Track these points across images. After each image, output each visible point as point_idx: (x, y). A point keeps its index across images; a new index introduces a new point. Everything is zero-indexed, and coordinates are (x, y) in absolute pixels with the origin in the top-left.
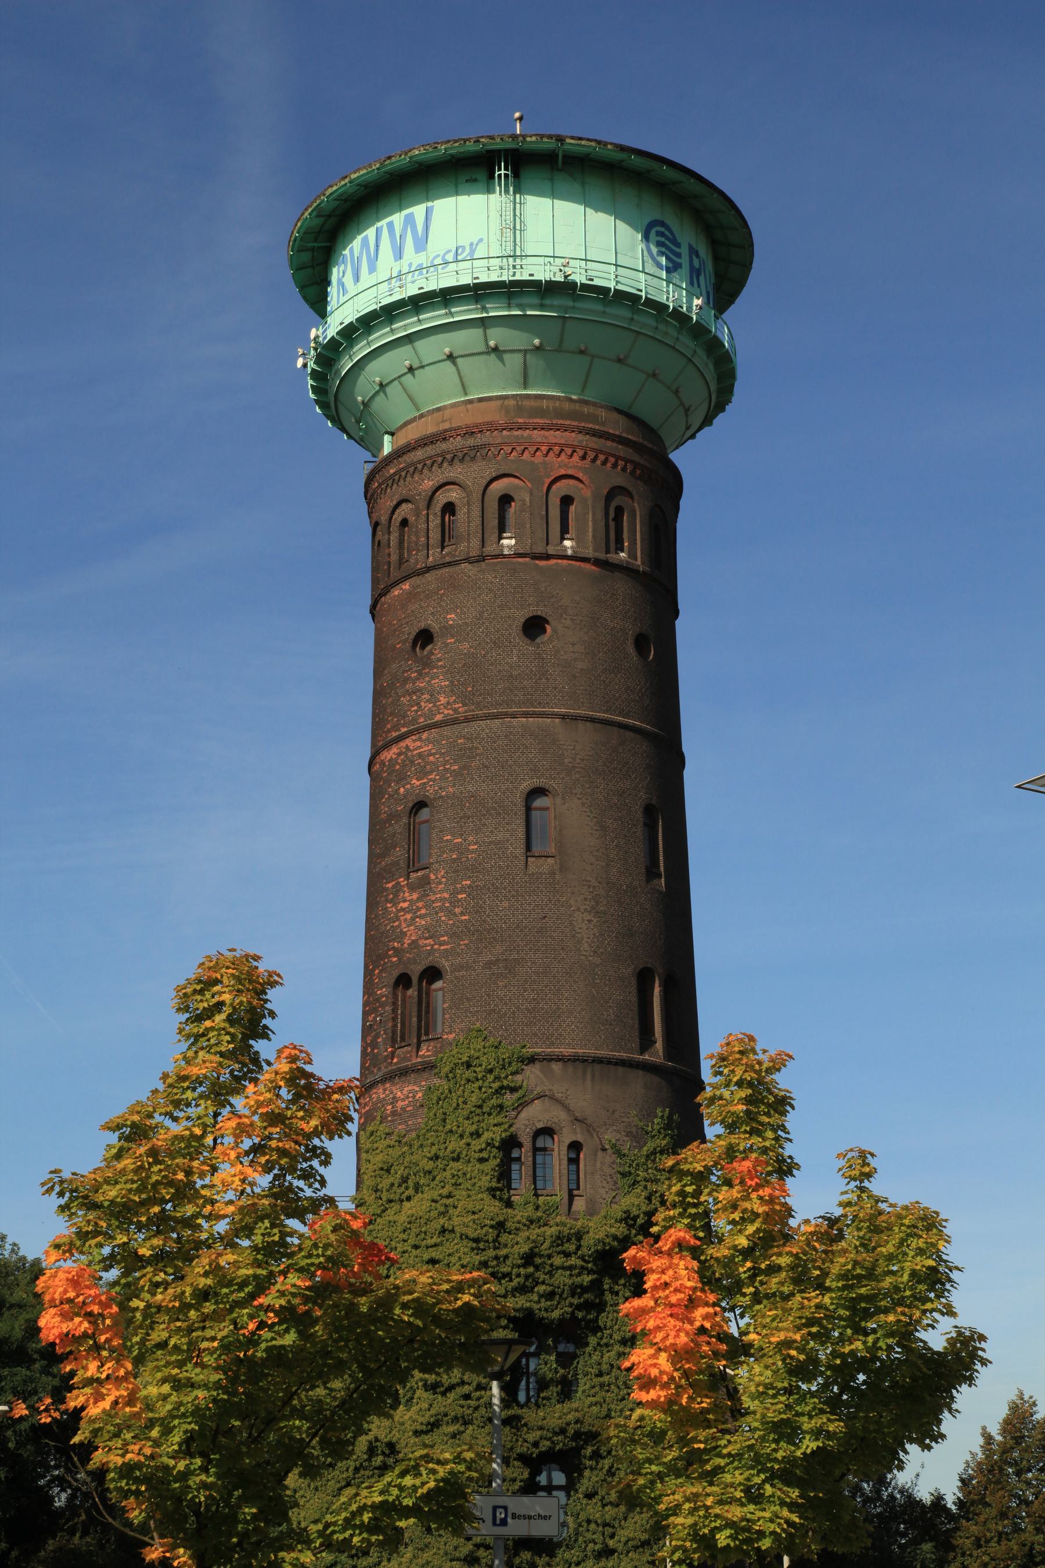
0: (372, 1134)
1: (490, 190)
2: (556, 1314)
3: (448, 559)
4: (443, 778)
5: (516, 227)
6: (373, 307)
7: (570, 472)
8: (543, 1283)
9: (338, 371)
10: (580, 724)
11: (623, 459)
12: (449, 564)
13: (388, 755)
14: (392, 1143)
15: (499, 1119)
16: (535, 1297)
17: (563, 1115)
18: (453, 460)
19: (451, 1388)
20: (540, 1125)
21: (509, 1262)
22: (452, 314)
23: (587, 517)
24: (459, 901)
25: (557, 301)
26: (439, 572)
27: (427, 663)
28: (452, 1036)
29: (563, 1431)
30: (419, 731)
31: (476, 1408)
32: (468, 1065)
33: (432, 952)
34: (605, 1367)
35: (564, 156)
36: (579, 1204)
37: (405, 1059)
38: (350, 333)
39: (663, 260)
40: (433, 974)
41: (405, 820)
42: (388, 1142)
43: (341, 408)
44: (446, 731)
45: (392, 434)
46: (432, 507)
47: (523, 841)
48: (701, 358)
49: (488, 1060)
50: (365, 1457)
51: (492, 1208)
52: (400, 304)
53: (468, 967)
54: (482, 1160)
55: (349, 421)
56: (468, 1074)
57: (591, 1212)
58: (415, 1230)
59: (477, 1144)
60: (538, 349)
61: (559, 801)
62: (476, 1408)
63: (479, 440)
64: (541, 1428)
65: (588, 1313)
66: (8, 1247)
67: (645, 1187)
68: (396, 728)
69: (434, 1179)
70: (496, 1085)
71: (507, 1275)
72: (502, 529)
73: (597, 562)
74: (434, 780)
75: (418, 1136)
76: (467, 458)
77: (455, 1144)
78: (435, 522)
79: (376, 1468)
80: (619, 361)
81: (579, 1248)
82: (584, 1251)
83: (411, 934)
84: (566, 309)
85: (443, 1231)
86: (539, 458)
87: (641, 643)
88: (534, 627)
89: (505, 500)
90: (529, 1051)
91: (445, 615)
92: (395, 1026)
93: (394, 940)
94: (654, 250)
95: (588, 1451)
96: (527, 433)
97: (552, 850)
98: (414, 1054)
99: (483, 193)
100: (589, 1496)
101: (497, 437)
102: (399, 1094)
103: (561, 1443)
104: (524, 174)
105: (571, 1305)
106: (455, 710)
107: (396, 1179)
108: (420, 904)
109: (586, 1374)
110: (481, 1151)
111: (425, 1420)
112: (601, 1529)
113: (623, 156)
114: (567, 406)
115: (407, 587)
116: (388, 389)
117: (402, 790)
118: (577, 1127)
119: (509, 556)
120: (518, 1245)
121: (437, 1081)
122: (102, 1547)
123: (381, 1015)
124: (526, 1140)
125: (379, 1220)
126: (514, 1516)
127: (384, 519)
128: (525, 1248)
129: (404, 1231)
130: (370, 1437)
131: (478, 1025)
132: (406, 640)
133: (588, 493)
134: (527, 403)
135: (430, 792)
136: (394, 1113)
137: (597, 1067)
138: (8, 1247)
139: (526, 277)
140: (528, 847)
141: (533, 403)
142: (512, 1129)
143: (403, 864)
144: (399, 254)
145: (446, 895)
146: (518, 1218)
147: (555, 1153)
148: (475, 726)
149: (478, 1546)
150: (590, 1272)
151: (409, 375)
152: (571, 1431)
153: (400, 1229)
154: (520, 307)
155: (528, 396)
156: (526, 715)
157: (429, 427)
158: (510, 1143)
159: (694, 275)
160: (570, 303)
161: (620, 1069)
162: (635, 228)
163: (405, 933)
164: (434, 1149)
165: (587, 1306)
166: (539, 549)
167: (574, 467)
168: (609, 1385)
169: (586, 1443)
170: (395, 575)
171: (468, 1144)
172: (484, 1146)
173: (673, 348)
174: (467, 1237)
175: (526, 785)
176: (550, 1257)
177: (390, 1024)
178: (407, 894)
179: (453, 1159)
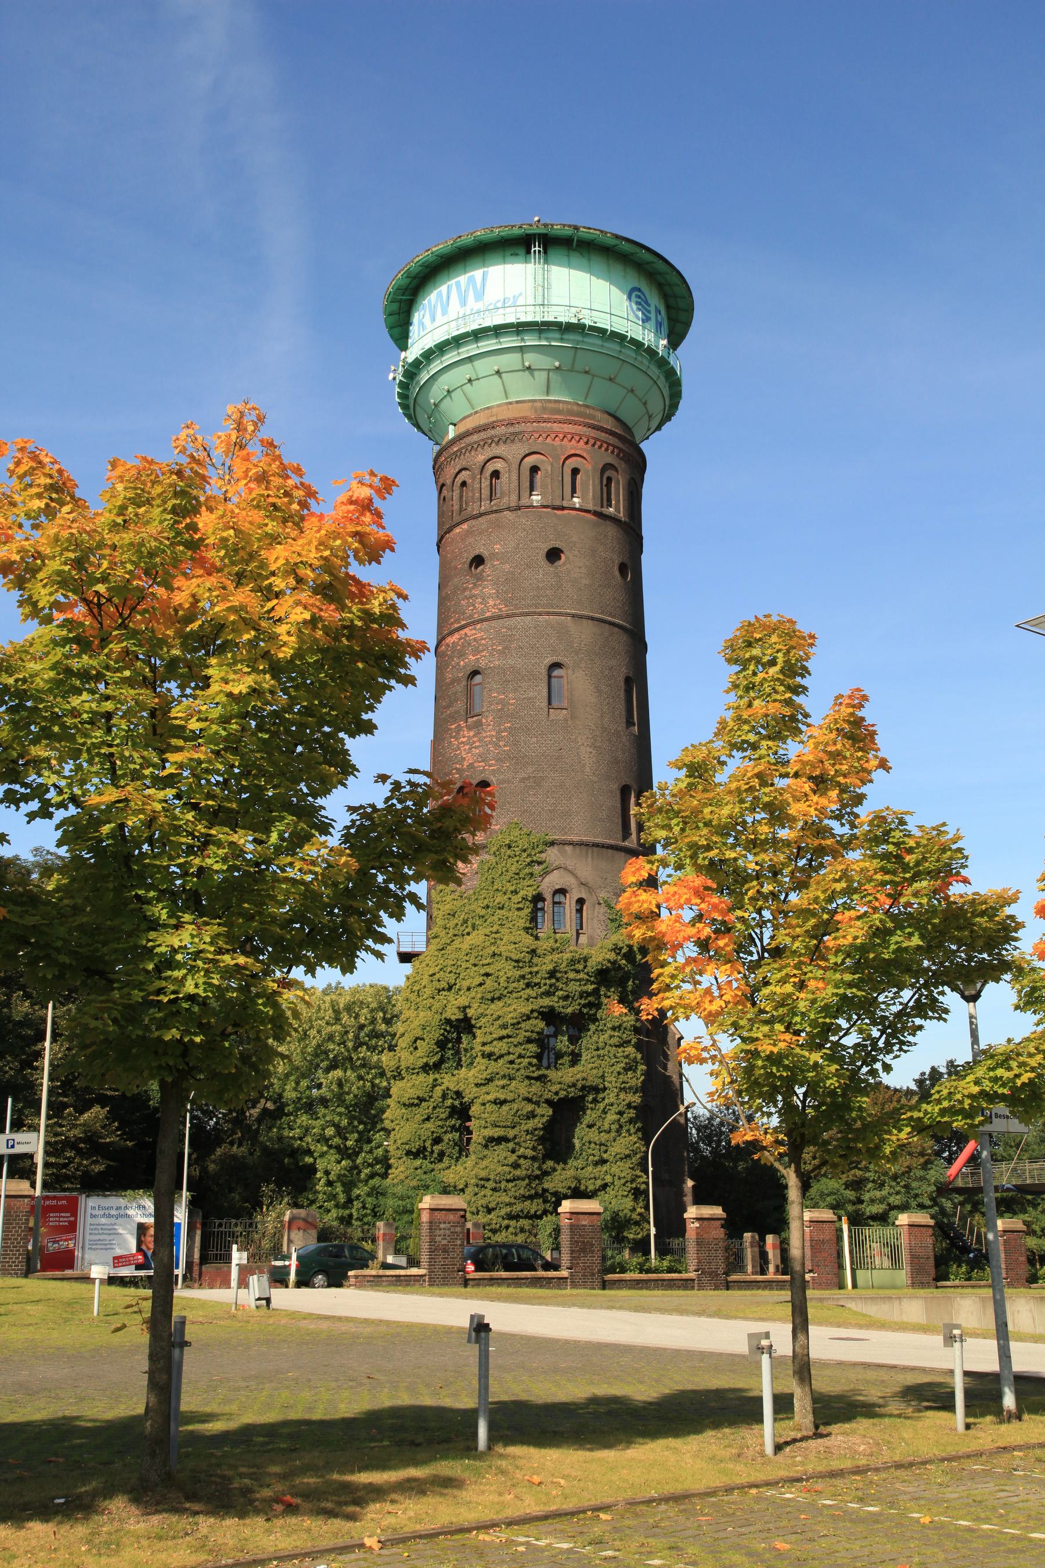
2: (569, 1010)
5: (545, 287)
9: (418, 382)
10: (584, 621)
12: (496, 511)
13: (450, 640)
15: (531, 882)
16: (556, 999)
17: (573, 880)
19: (501, 1056)
27: (480, 578)
29: (574, 1085)
32: (510, 847)
33: (484, 770)
34: (601, 1045)
36: (583, 939)
38: (429, 355)
39: (640, 314)
41: (464, 683)
43: (418, 409)
44: (493, 623)
48: (662, 382)
49: (523, 843)
51: (528, 940)
52: (466, 335)
53: (508, 782)
54: (519, 909)
55: (422, 418)
56: (509, 852)
57: (591, 944)
58: (474, 954)
60: (557, 368)
61: (570, 672)
68: (457, 621)
70: (528, 860)
72: (532, 488)
73: (596, 514)
77: (500, 899)
78: (486, 483)
80: (611, 379)
82: (589, 969)
83: (469, 759)
84: (578, 342)
85: (494, 955)
87: (623, 568)
88: (553, 555)
89: (534, 469)
94: (635, 307)
95: (590, 1098)
97: (565, 705)
100: (590, 1126)
101: (530, 427)
103: (573, 1093)
104: (550, 251)
107: (458, 920)
111: (484, 1076)
114: (575, 408)
120: (545, 965)
121: (487, 857)
122: (251, 1154)
124: (548, 896)
127: (449, 482)
128: (550, 967)
130: (444, 1087)
133: (590, 467)
134: (549, 405)
135: (482, 664)
137: (595, 849)
139: (551, 319)
140: (550, 703)
141: (553, 405)
143: (463, 712)
144: (464, 302)
147: (567, 906)
148: (514, 620)
149: (519, 1157)
150: (592, 983)
152: (579, 1085)
154: (547, 339)
155: (550, 401)
156: (548, 614)
157: (481, 420)
158: (538, 898)
159: (659, 325)
160: (580, 338)
164: (486, 902)
165: (590, 1005)
166: (558, 503)
170: (457, 518)
175: (548, 661)
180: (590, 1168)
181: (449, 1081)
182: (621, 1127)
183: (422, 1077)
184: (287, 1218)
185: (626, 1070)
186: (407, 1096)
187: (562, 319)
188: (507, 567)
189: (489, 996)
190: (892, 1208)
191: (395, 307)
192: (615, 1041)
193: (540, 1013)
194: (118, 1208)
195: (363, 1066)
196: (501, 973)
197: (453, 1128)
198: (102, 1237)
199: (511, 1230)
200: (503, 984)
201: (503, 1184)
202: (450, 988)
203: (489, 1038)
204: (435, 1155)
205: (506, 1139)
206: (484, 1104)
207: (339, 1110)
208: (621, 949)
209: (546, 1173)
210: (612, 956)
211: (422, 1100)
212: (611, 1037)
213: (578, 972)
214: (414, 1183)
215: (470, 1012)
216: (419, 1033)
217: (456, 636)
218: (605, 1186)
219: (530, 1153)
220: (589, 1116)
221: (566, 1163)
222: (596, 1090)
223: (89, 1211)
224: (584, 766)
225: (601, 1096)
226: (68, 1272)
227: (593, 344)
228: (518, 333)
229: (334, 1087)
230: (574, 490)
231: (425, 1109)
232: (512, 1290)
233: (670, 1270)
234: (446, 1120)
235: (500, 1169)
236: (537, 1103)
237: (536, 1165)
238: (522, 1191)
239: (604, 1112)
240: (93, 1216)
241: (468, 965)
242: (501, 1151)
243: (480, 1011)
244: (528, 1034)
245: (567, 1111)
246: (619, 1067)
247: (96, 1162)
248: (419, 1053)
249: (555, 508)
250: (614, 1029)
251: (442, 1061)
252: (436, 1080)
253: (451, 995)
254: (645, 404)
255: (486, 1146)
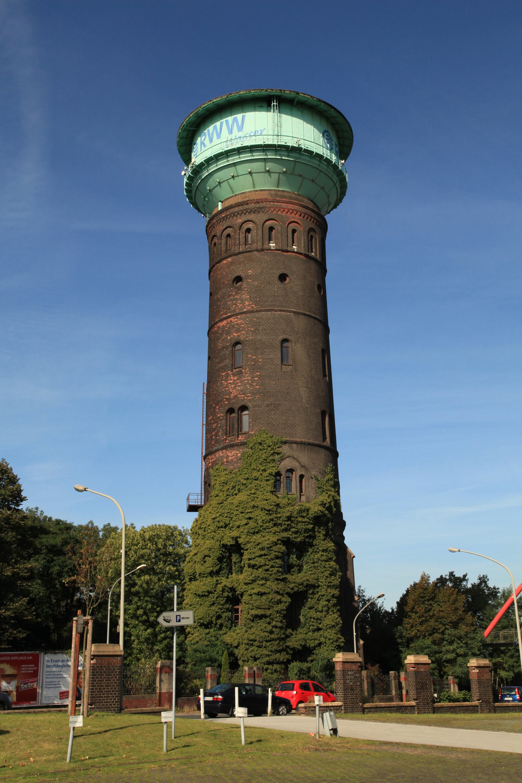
0: (217, 469)
1: (268, 110)
3: (248, 250)
4: (247, 333)
5: (279, 125)
6: (222, 151)
7: (295, 220)
8: (294, 527)
9: (201, 177)
10: (301, 316)
11: (314, 218)
12: (249, 252)
13: (221, 324)
14: (227, 473)
16: (290, 533)
17: (297, 464)
18: (250, 212)
19: (260, 567)
20: (289, 468)
21: (281, 519)
22: (253, 156)
23: (301, 237)
24: (255, 380)
25: (294, 155)
26: (245, 254)
27: (240, 289)
28: (253, 432)
29: (302, 584)
30: (236, 315)
31: (271, 575)
32: (261, 444)
33: (244, 399)
34: (315, 560)
35: (297, 102)
36: (303, 498)
37: (232, 441)
39: (328, 145)
40: (244, 408)
42: (225, 472)
44: (249, 315)
45: (222, 202)
46: (241, 230)
47: (280, 359)
49: (269, 442)
50: (221, 593)
51: (274, 498)
52: (233, 150)
53: (259, 406)
54: (267, 480)
56: (260, 447)
57: (308, 501)
59: (266, 474)
60: (284, 172)
61: (293, 344)
62: (271, 575)
63: (261, 205)
64: (294, 583)
65: (310, 539)
66: (39, 512)
67: (327, 493)
69: (247, 487)
70: (272, 452)
71: (281, 524)
72: (270, 239)
73: (306, 255)
74: (244, 334)
75: (239, 471)
76: (256, 212)
77: (255, 474)
78: (242, 236)
79: (225, 597)
80: (313, 181)
81: (308, 514)
83: (234, 393)
84: (297, 158)
85: (254, 506)
86: (284, 214)
88: (283, 277)
89: (271, 229)
90: (284, 439)
91: (248, 271)
92: (227, 428)
93: (226, 395)
94: (326, 141)
95: (311, 592)
96: (280, 204)
98: (236, 439)
99: (266, 112)
101: (269, 205)
102: (230, 454)
103: (302, 588)
104: (280, 106)
105: (304, 536)
106: (252, 307)
108: (238, 381)
109: (307, 563)
110: (267, 476)
111: (251, 578)
112: (315, 621)
113: (319, 103)
115: (230, 260)
116: (222, 185)
117: (229, 337)
118: (303, 469)
119: (273, 250)
120: (285, 513)
121: (247, 450)
123: (220, 424)
124: (283, 473)
125: (225, 502)
126: (183, 618)
127: (218, 234)
128: (288, 514)
129: (237, 507)
130: (222, 585)
131: (264, 428)
132: (230, 280)
133: (302, 229)
134: (279, 193)
135: (242, 338)
136: (227, 462)
137: (309, 446)
138: (39, 512)
139: (283, 144)
140: (282, 362)
142: (279, 469)
144: (231, 132)
145: (250, 378)
146: (284, 502)
147: (294, 479)
149: (273, 627)
150: (312, 524)
151: (232, 179)
153: (234, 506)
154: (280, 155)
155: (279, 191)
156: (281, 311)
157: (240, 199)
158: (278, 474)
160: (299, 156)
161: (317, 448)
162: (320, 132)
163: (231, 393)
164: (247, 476)
165: (310, 537)
166: (285, 248)
167: (297, 219)
168: (317, 567)
169: (310, 589)
170: (224, 255)
171: (261, 474)
172: (268, 475)
173: (331, 178)
174: (265, 509)
175: (281, 337)
176: (297, 518)
177: (225, 427)
178: (232, 377)
179: (255, 480)
180: (310, 634)
181: (225, 582)
182: (329, 609)
183: (209, 579)
184: (159, 666)
185: (331, 575)
186: (201, 590)
187: (290, 144)
188: (256, 283)
189: (252, 531)
190: (458, 655)
191: (185, 134)
192: (324, 558)
193: (282, 541)
194: (63, 661)
195: (161, 573)
196: (259, 518)
197: (228, 610)
198: (53, 680)
199: (269, 671)
200: (260, 524)
201: (264, 644)
202: (226, 526)
203: (253, 556)
204: (218, 626)
205: (265, 616)
206: (251, 595)
207: (146, 599)
208: (326, 504)
209: (287, 637)
210: (321, 508)
211: (210, 592)
212: (322, 556)
213: (303, 517)
214: (206, 643)
215: (240, 541)
216: (207, 552)
217: (225, 322)
218: (320, 644)
219: (279, 624)
220: (310, 602)
221: (297, 631)
222: (314, 587)
223: (46, 663)
224: (302, 398)
225: (316, 590)
226: (33, 704)
227: (305, 160)
228: (263, 151)
229: (145, 585)
230: (293, 242)
231: (212, 598)
232: (398, 715)
233: (465, 700)
234: (223, 605)
235: (262, 634)
236: (282, 595)
237: (283, 631)
238: (275, 648)
239: (318, 600)
240: (48, 666)
241: (238, 512)
242: (262, 624)
243: (247, 540)
244: (276, 553)
245: (299, 598)
246: (327, 573)
247: (20, 632)
248: (207, 565)
249: (284, 251)
250: (323, 551)
251: (220, 569)
252: (217, 581)
253: (227, 531)
254: (328, 196)
255: (253, 621)
